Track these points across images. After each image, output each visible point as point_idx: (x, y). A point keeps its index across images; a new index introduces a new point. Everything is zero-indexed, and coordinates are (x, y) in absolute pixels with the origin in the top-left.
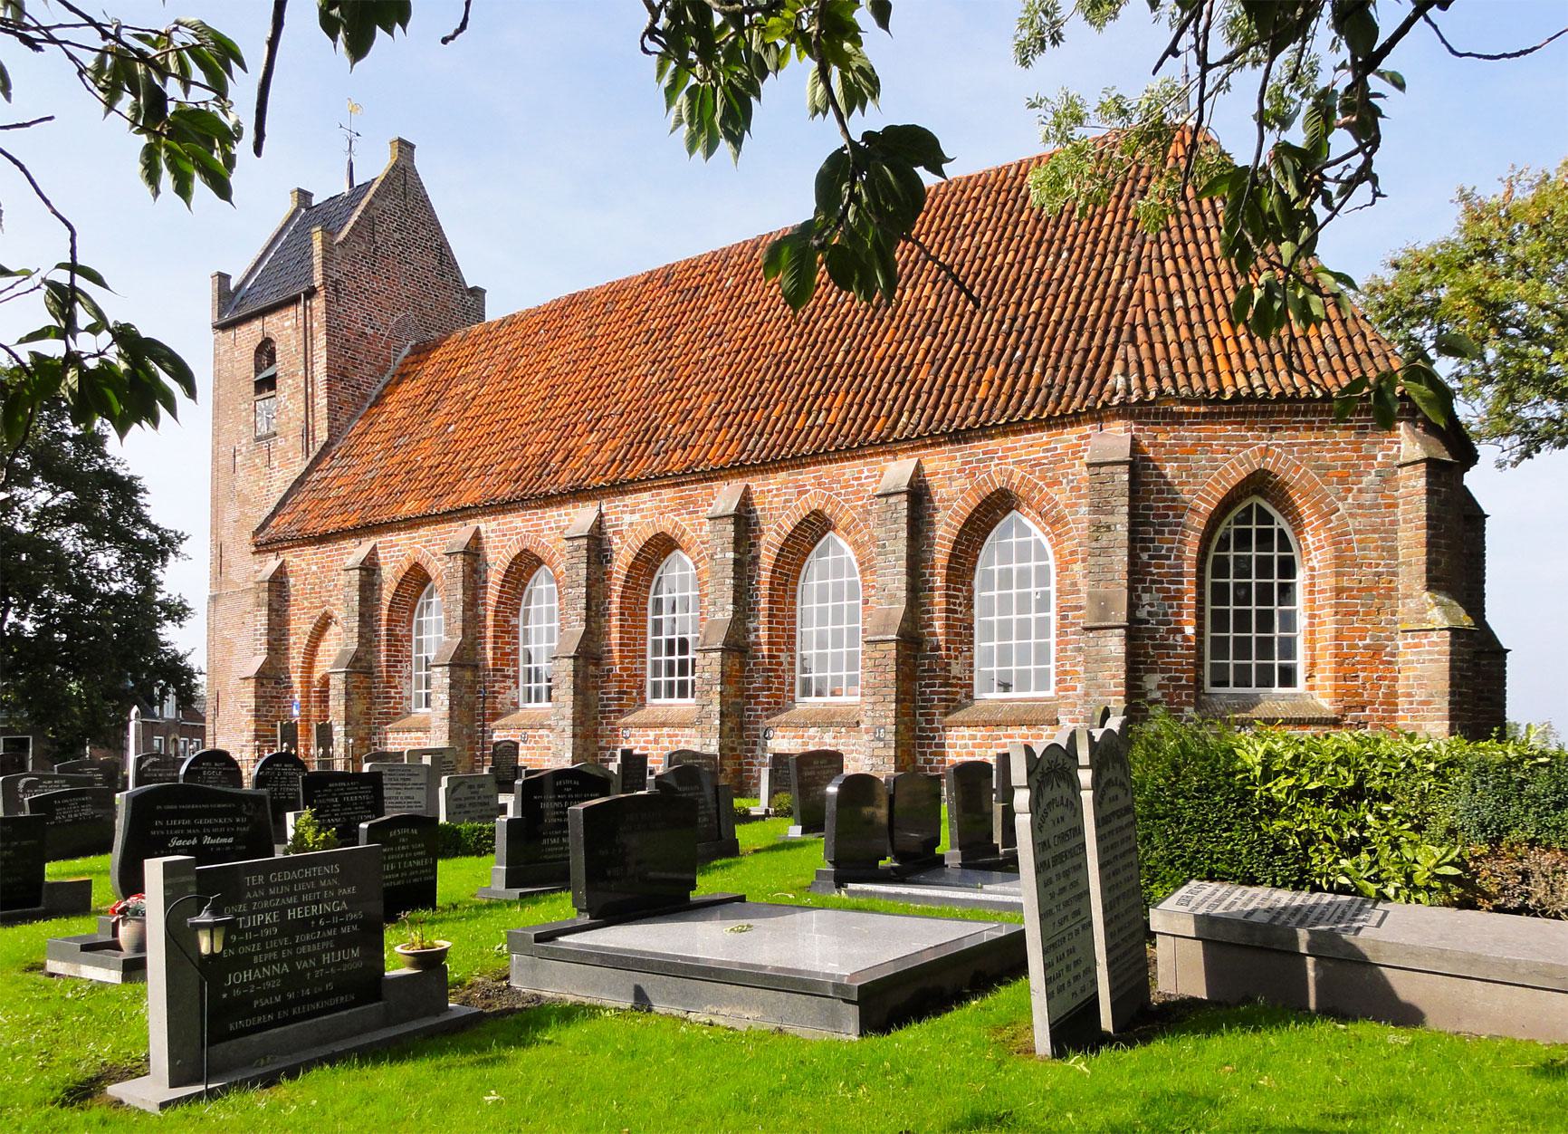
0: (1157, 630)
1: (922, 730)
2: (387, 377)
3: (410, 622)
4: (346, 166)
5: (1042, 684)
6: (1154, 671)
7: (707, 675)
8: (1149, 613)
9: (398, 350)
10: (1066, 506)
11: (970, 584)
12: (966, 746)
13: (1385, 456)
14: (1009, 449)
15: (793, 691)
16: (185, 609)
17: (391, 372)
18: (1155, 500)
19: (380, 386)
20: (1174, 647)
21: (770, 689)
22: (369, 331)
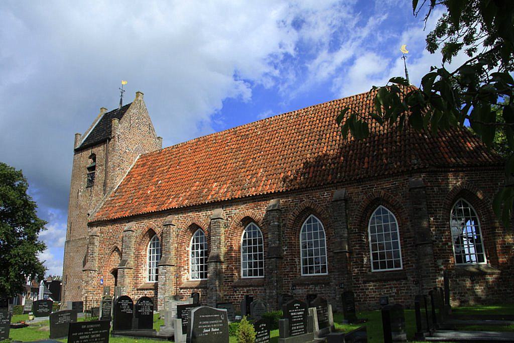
0: (439, 244)
1: (355, 284)
2: (132, 166)
3: (146, 249)
4: (120, 100)
5: (398, 265)
6: (440, 258)
7: (270, 267)
8: (436, 238)
9: (135, 157)
10: (402, 203)
11: (367, 231)
12: (373, 289)
13: (501, 184)
14: (379, 184)
15: (300, 272)
16: (44, 247)
17: (133, 164)
18: (433, 200)
19: (130, 169)
20: (445, 250)
21: (292, 272)
22: (127, 151)
